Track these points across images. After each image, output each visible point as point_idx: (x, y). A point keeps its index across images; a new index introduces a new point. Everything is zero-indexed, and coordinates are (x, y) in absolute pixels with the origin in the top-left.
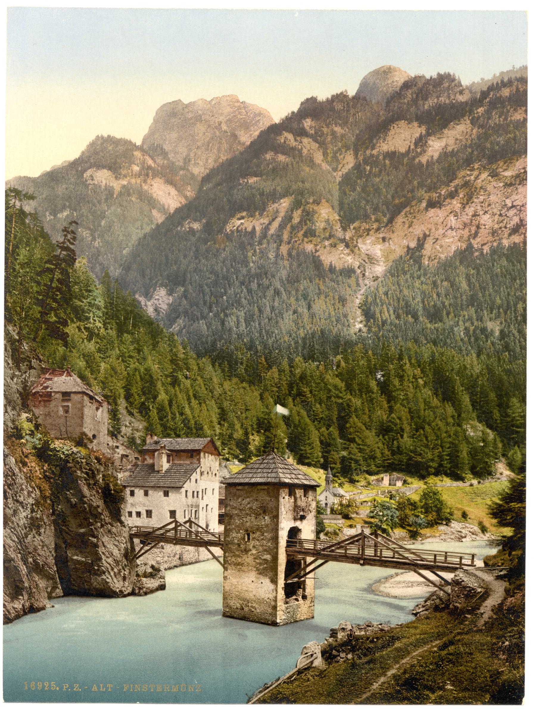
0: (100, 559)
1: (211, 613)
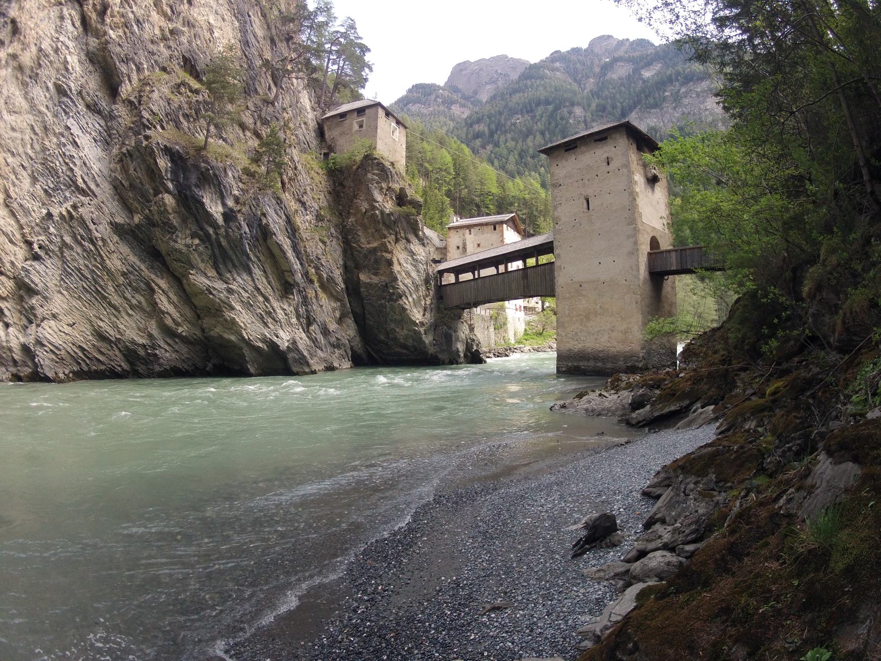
0: (396, 279)
1: (548, 376)
